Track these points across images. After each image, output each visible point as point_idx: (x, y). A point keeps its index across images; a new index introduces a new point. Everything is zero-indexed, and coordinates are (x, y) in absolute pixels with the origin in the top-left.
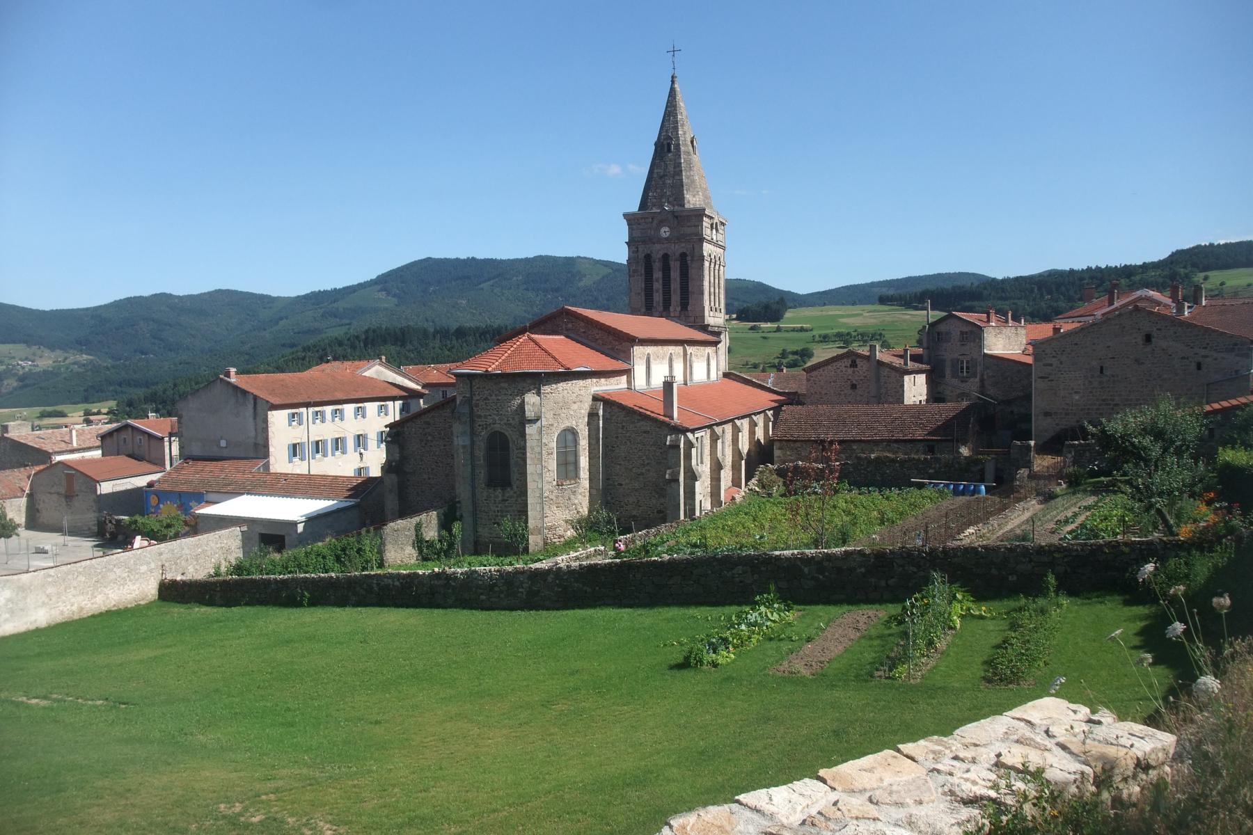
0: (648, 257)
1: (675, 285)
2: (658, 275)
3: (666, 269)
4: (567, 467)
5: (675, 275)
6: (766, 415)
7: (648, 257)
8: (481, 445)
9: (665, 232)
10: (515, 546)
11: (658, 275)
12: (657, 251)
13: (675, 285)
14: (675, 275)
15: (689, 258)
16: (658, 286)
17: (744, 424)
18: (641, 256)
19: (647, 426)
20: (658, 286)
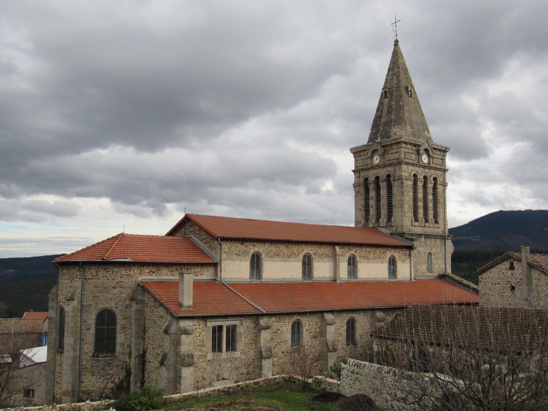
0: (366, 180)
1: (384, 202)
2: (372, 194)
3: (378, 189)
4: (383, 196)
5: (384, 192)
6: (351, 326)
7: (366, 180)
8: (91, 319)
9: (376, 160)
10: (356, 278)
11: (372, 194)
12: (371, 175)
13: (384, 202)
14: (384, 192)
15: (392, 179)
16: (372, 202)
17: (309, 325)
18: (362, 180)
19: (43, 364)
20: (372, 202)
